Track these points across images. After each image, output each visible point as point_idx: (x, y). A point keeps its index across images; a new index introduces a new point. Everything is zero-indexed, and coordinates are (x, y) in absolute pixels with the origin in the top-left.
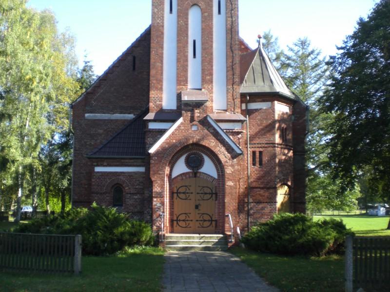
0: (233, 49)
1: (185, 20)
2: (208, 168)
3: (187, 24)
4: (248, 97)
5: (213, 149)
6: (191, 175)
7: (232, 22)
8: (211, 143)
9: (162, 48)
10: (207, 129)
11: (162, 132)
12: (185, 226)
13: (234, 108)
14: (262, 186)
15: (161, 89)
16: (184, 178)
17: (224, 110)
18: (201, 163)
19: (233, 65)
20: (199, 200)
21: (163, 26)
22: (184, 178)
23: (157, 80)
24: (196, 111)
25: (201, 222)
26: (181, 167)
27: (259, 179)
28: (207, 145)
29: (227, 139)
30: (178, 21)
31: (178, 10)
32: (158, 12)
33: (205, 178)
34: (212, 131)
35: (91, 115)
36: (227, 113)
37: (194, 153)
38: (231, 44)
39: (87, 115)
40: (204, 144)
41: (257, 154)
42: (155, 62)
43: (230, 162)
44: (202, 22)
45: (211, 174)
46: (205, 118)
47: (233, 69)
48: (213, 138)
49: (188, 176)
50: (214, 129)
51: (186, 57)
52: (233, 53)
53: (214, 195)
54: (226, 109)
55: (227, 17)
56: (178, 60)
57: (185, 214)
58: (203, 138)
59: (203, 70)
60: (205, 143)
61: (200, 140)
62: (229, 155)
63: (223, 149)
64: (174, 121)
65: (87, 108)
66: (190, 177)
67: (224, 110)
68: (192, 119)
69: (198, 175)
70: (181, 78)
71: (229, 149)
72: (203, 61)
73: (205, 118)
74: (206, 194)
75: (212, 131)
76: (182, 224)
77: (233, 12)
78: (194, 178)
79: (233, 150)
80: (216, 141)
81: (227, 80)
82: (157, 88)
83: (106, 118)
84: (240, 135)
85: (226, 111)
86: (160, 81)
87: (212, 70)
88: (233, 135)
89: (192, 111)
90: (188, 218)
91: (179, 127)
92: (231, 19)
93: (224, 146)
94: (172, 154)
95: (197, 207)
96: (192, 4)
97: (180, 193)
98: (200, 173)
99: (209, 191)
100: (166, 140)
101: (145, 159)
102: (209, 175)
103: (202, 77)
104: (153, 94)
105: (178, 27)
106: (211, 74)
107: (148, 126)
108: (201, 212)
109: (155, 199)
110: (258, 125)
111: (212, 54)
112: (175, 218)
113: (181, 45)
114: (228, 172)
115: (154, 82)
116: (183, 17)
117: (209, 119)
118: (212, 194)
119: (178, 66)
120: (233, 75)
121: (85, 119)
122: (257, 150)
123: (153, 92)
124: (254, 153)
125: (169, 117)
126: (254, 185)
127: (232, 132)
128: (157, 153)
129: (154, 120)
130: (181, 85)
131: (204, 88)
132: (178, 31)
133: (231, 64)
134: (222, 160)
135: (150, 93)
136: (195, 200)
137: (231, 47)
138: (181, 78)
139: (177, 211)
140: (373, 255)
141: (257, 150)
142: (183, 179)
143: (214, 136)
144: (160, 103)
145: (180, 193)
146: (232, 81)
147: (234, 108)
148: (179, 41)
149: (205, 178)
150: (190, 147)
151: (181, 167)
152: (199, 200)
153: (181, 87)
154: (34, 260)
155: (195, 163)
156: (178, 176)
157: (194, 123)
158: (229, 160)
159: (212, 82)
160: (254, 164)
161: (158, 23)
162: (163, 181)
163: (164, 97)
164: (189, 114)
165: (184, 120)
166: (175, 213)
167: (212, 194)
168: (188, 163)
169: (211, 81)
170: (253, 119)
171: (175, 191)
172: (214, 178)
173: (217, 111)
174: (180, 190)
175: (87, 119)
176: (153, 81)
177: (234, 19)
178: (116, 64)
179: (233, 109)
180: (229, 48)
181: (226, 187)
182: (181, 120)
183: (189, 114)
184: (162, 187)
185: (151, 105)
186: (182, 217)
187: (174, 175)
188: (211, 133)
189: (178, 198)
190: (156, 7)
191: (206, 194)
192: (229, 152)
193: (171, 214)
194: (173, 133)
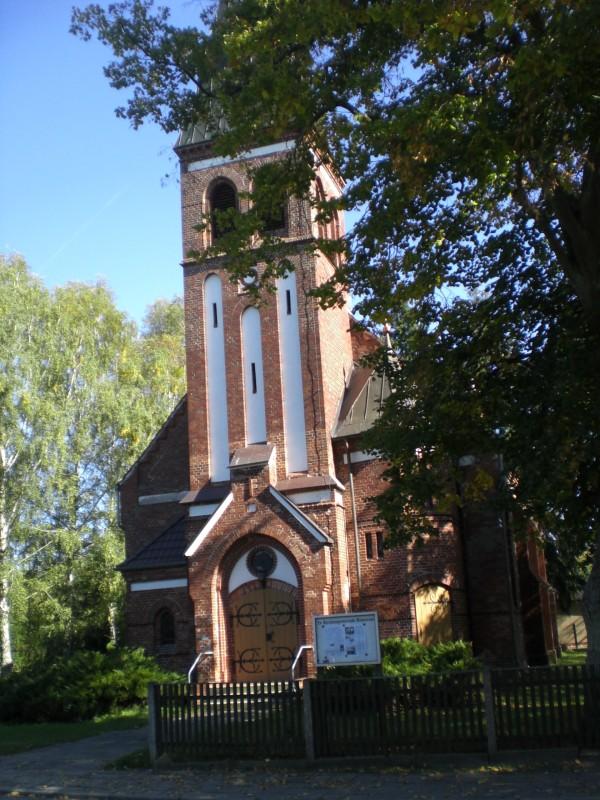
0: (312, 368)
1: (236, 334)
2: (283, 572)
3: (239, 341)
4: (347, 445)
5: (280, 540)
6: (257, 585)
7: (308, 324)
8: (278, 530)
9: (204, 384)
10: (271, 508)
11: (205, 519)
12: (252, 670)
13: (319, 467)
14: (384, 592)
15: (206, 451)
16: (247, 590)
17: (303, 472)
18: (271, 564)
19: (313, 395)
20: (272, 625)
21: (203, 351)
22: (247, 590)
23: (198, 438)
24: (252, 481)
25: (278, 663)
26: (242, 575)
27: (379, 580)
28: (271, 535)
29: (302, 521)
30: (226, 338)
31: (224, 319)
32: (195, 328)
33: (279, 588)
34: (279, 510)
35: (148, 497)
36: (308, 476)
37: (257, 549)
38: (308, 361)
39: (141, 499)
40: (266, 533)
41: (374, 538)
42: (195, 410)
43: (309, 559)
44: (263, 332)
45: (287, 581)
46: (267, 490)
47: (313, 401)
48: (281, 521)
49: (252, 587)
50: (282, 507)
51: (240, 393)
52: (312, 374)
53: (295, 616)
54: (306, 469)
55: (300, 316)
56: (229, 400)
57: (252, 650)
58: (265, 522)
59: (268, 410)
60: (267, 531)
61: (260, 526)
62: (306, 546)
63: (297, 538)
64: (220, 501)
65: (142, 487)
66: (255, 589)
67: (303, 472)
68: (247, 496)
69: (268, 584)
70: (236, 431)
71: (307, 537)
72: (267, 394)
73: (267, 490)
74: (282, 614)
75: (279, 510)
76: (248, 666)
77: (308, 307)
78: (262, 591)
79: (312, 537)
80: (287, 526)
81: (307, 421)
82: (200, 451)
83: (170, 500)
84: (329, 511)
85: (306, 472)
86: (203, 439)
87: (281, 408)
88: (317, 512)
89: (247, 482)
90: (256, 657)
91: (228, 509)
92: (305, 319)
93: (298, 533)
94: (225, 553)
95: (269, 637)
96: (244, 307)
97: (242, 616)
98: (271, 579)
99: (286, 609)
100: (211, 532)
101: (182, 567)
102: (284, 583)
103: (267, 422)
104: (194, 461)
105: (226, 347)
106: (280, 416)
107: (188, 513)
108: (277, 645)
109: (199, 630)
110: (371, 487)
111: (279, 382)
112: (237, 658)
113: (232, 375)
114: (307, 576)
115: (195, 440)
116: (232, 329)
117: (272, 491)
118: (291, 613)
119: (229, 411)
120: (315, 411)
121: (140, 506)
122: (373, 530)
123: (194, 458)
124: (368, 536)
125: (213, 494)
126: (372, 591)
127: (316, 508)
128: (199, 555)
129: (197, 503)
130: (235, 440)
131: (270, 440)
132: (226, 354)
133: (310, 394)
134: (296, 556)
135: (191, 460)
136: (266, 627)
137: (308, 366)
138: (236, 431)
139: (239, 647)
140: (573, 703)
141: (373, 530)
142: (245, 593)
143: (281, 517)
144: (205, 473)
145: (242, 616)
146: (312, 420)
147: (319, 467)
148: (228, 370)
149: (279, 588)
150: (250, 540)
151: (242, 575)
152: (272, 625)
153: (235, 443)
154: (428, 731)
155: (262, 564)
156: (238, 589)
157: (251, 500)
158: (308, 555)
159: (281, 428)
160: (370, 555)
161: (197, 346)
162: (209, 599)
163: (212, 464)
164: (242, 486)
165: (236, 497)
166: (236, 649)
167: (291, 613)
168: (252, 566)
169: (280, 427)
170: (362, 478)
171: (235, 613)
172: (294, 587)
173: (293, 475)
174: (243, 612)
175: (143, 506)
176: (194, 441)
177: (310, 318)
178: (179, 410)
179: (316, 469)
180: (306, 367)
181: (305, 600)
182: (230, 498)
183: (242, 486)
184: (209, 608)
185: (193, 478)
186: (248, 656)
187: (233, 585)
188: (278, 514)
189: (240, 626)
190: (192, 322)
191: (282, 614)
192: (307, 543)
193: (231, 650)
194: (220, 521)
